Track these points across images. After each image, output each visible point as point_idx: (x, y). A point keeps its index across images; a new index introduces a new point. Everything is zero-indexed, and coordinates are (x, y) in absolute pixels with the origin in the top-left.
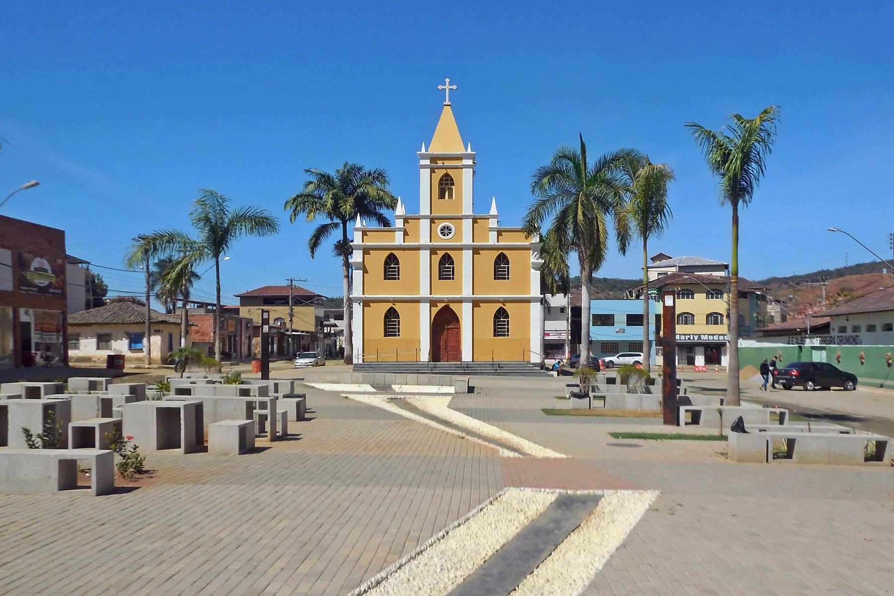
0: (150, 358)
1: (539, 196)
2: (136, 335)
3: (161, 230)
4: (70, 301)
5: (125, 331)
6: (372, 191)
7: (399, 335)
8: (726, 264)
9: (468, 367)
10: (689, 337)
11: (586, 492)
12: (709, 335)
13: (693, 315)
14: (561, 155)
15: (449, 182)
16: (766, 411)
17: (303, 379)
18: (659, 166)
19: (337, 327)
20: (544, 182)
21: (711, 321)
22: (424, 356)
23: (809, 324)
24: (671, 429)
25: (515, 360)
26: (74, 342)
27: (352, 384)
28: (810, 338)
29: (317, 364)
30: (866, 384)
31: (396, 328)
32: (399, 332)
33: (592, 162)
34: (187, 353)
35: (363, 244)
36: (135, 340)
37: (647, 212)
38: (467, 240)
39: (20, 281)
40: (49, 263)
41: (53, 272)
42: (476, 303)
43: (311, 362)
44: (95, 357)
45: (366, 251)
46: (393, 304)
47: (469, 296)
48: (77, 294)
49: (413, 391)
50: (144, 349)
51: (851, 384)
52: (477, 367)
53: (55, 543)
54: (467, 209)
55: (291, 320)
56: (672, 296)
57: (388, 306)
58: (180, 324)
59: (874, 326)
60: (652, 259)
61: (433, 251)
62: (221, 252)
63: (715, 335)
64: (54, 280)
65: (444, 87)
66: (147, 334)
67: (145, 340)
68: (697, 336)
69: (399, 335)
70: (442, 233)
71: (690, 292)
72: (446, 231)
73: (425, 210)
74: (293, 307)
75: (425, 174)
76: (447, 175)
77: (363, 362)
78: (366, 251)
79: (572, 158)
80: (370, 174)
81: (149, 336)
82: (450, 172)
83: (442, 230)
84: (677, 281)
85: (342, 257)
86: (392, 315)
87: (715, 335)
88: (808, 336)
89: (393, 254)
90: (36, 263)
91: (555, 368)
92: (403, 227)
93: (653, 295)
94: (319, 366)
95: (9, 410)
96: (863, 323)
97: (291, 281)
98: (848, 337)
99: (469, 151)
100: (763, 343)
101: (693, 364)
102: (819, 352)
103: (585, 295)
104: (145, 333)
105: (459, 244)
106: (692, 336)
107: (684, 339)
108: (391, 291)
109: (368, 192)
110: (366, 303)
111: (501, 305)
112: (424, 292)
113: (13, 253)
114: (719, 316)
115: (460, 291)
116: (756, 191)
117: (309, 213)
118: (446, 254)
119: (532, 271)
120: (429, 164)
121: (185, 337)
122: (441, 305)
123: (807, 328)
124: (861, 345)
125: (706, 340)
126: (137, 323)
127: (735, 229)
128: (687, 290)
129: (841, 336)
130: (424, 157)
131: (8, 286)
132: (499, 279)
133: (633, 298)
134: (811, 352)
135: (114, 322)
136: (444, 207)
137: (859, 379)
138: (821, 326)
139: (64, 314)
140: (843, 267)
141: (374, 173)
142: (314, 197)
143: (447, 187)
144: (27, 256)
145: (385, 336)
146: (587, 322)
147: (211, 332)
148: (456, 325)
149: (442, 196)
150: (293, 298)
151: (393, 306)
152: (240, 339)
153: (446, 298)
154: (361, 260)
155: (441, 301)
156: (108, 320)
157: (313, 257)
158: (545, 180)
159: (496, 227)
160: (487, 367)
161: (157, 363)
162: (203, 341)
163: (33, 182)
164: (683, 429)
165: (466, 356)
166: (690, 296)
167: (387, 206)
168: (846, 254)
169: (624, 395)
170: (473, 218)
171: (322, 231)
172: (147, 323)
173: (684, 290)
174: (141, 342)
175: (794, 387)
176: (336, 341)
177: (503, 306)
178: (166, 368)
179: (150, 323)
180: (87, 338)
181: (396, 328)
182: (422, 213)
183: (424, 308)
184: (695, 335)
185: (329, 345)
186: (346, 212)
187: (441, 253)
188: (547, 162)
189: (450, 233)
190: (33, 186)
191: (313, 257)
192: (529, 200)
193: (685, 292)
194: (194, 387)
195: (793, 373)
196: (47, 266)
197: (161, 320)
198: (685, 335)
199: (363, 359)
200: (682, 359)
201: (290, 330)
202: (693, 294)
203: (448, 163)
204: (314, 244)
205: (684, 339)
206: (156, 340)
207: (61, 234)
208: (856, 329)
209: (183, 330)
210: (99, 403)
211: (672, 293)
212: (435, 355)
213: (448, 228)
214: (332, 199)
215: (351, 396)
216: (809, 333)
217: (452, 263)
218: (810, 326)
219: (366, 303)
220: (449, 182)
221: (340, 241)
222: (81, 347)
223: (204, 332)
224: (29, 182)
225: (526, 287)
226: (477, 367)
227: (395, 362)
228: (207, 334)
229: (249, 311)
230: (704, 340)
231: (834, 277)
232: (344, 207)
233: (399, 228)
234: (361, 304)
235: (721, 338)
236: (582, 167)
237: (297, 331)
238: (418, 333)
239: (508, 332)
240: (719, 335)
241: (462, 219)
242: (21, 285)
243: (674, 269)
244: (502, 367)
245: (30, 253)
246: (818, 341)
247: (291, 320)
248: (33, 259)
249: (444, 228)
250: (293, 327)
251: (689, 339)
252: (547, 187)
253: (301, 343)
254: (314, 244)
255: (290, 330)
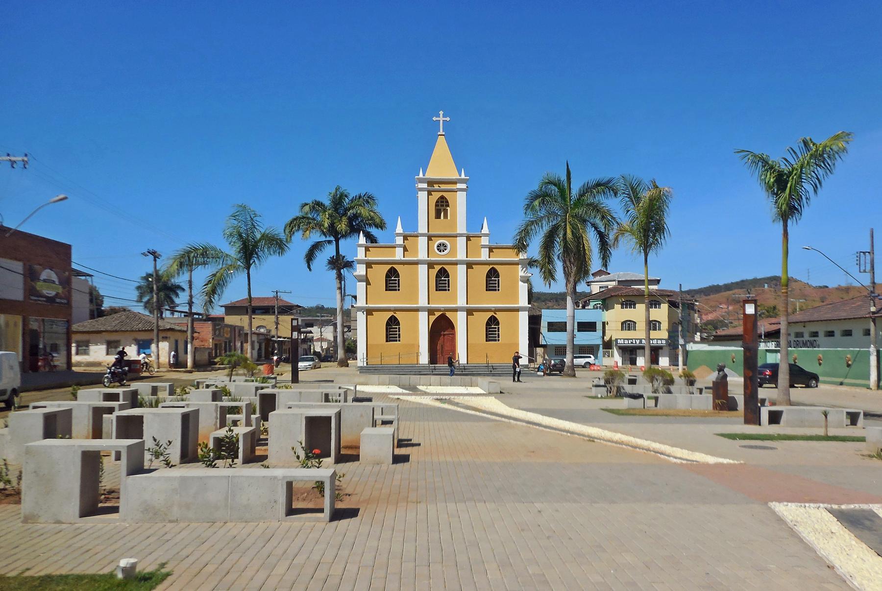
0: (158, 362)
1: (530, 217)
2: (143, 341)
3: (196, 244)
4: (75, 312)
5: (134, 338)
6: (364, 211)
7: (399, 341)
8: (659, 279)
9: (465, 369)
10: (632, 341)
11: (852, 506)
12: (624, 339)
13: (635, 323)
14: (547, 181)
15: (445, 204)
16: (843, 411)
17: (333, 381)
18: (667, 189)
19: (312, 333)
20: (535, 205)
21: (626, 327)
22: (424, 358)
23: (763, 330)
24: (752, 429)
25: (506, 362)
26: (84, 348)
27: (379, 385)
28: (765, 342)
29: (315, 367)
30: (825, 382)
31: (396, 334)
32: (399, 337)
33: (575, 190)
34: (236, 358)
35: (366, 258)
36: (143, 346)
37: (649, 231)
38: (461, 255)
39: (30, 291)
40: (57, 274)
41: (61, 283)
42: (470, 312)
43: (310, 365)
44: (105, 362)
45: (369, 265)
46: (394, 313)
47: (463, 306)
48: (80, 303)
49: (474, 392)
50: (152, 354)
51: (814, 382)
52: (472, 369)
53: (83, 534)
54: (461, 227)
55: (277, 328)
56: (754, 305)
57: (389, 314)
58: (186, 332)
59: (833, 332)
60: (593, 274)
61: (431, 265)
62: (251, 265)
63: (654, 339)
64: (60, 290)
65: (438, 119)
66: (155, 340)
67: (153, 346)
68: (639, 341)
69: (399, 341)
70: (438, 249)
71: (657, 303)
72: (442, 248)
73: (422, 228)
74: (278, 316)
75: (422, 196)
76: (442, 197)
77: (367, 365)
78: (369, 265)
79: (557, 184)
80: (360, 197)
81: (158, 342)
82: (445, 194)
83: (438, 246)
84: (621, 293)
85: (335, 271)
86: (393, 322)
87: (654, 339)
88: (762, 340)
89: (394, 268)
90: (46, 274)
91: (540, 369)
92: (402, 243)
93: (599, 306)
94: (317, 368)
95: (145, 420)
96: (821, 329)
97: (277, 293)
98: (805, 342)
99: (463, 176)
100: (715, 347)
101: (635, 364)
102: (774, 354)
103: (570, 304)
104: (153, 340)
105: (454, 259)
106: (634, 340)
107: (627, 343)
108: (392, 301)
109: (360, 213)
110: (369, 312)
111: (492, 314)
112: (423, 302)
113: (24, 264)
114: (657, 323)
115: (455, 301)
116: (806, 211)
117: (305, 232)
118: (392, 268)
119: (521, 283)
120: (426, 187)
121: (192, 343)
122: (438, 314)
123: (761, 333)
124: (818, 348)
125: (622, 344)
126: (145, 331)
127: (785, 244)
128: (630, 301)
129: (798, 341)
130: (421, 181)
131: (17, 294)
132: (490, 290)
133: (580, 308)
134: (766, 354)
135: (123, 329)
136: (440, 226)
137: (821, 378)
138: (774, 332)
139: (69, 323)
140: (730, 282)
141: (364, 196)
142: (308, 218)
143: (442, 208)
144: (37, 267)
145: (387, 341)
146: (572, 328)
147: (210, 338)
148: (452, 332)
149: (438, 216)
150: (279, 307)
151: (395, 315)
152: (233, 345)
153: (493, 307)
154: (364, 273)
155: (438, 310)
156: (117, 328)
157: (310, 270)
158: (536, 203)
159: (488, 244)
160: (482, 369)
161: (165, 367)
162: (202, 347)
163: (62, 196)
164: (765, 428)
165: (462, 357)
166: (657, 306)
167: (377, 226)
168: (808, 269)
169: (676, 396)
170: (466, 236)
171: (316, 247)
172: (155, 331)
173: (627, 301)
174: (149, 348)
175: (765, 385)
176: (310, 345)
177: (494, 315)
178: (174, 371)
179: (159, 330)
180: (97, 345)
181: (396, 334)
182: (459, 231)
183: (423, 317)
184: (636, 339)
185: (306, 349)
186: (342, 230)
187: (437, 268)
188: (535, 187)
189: (446, 249)
190: (61, 200)
191: (310, 270)
192: (520, 219)
193: (628, 303)
194: (279, 392)
195: (767, 373)
196: (54, 277)
197: (168, 328)
198: (628, 339)
199: (367, 363)
200: (625, 360)
201: (276, 337)
202: (635, 305)
203: (443, 187)
204: (310, 257)
205: (627, 343)
206: (164, 346)
207: (68, 247)
208: (815, 334)
209: (189, 337)
210: (217, 411)
211: (753, 302)
212: (433, 359)
213: (443, 244)
214: (328, 219)
215: (401, 397)
216: (763, 338)
217: (448, 276)
218: (764, 332)
219: (369, 312)
220: (445, 204)
221: (333, 256)
222: (91, 353)
223: (203, 338)
224: (57, 196)
225: (515, 297)
226: (472, 369)
227: (397, 364)
228: (206, 341)
229: (241, 320)
230: (620, 344)
231: (723, 290)
232: (340, 225)
233: (399, 245)
234: (365, 313)
235: (659, 342)
236: (567, 192)
237: (280, 337)
238: (417, 338)
239: (499, 337)
240: (657, 339)
241: (456, 237)
242: (32, 296)
243: (614, 283)
244: (496, 369)
245: (40, 265)
246: (774, 344)
247: (277, 328)
248: (42, 271)
249: (440, 244)
250: (279, 335)
251: (632, 343)
252: (538, 208)
253: (284, 348)
254: (310, 257)
255: (276, 337)
